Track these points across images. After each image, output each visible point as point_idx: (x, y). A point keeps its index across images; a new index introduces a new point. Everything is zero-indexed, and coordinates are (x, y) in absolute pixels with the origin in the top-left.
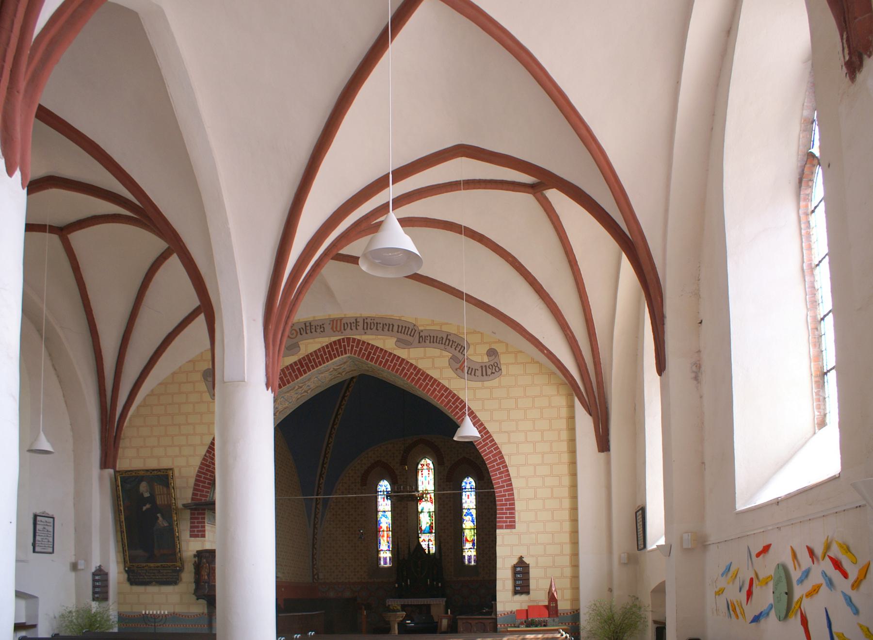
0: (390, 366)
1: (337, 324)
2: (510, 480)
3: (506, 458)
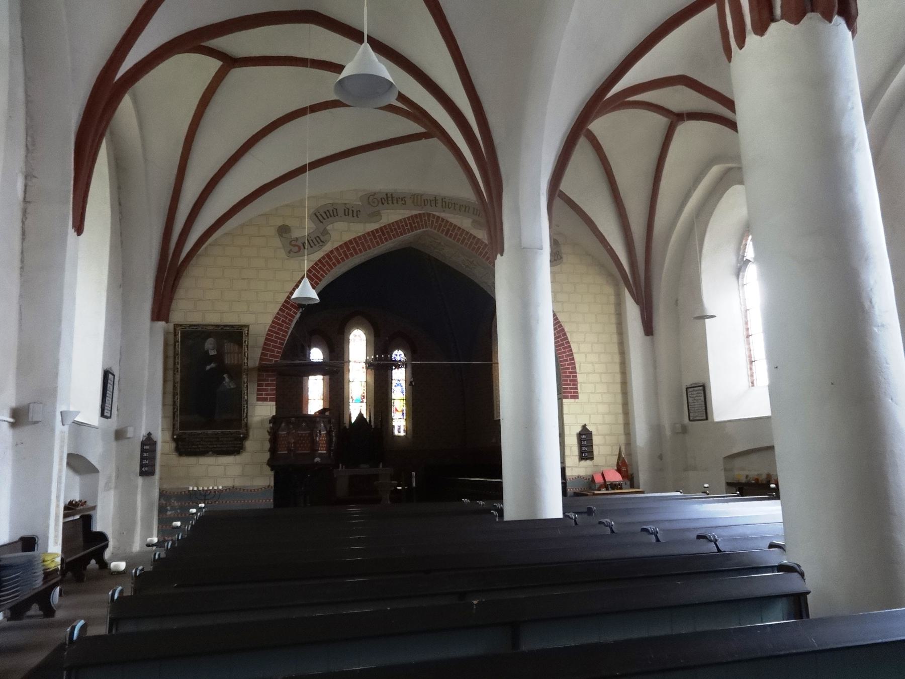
1: (418, 199)
2: (572, 355)
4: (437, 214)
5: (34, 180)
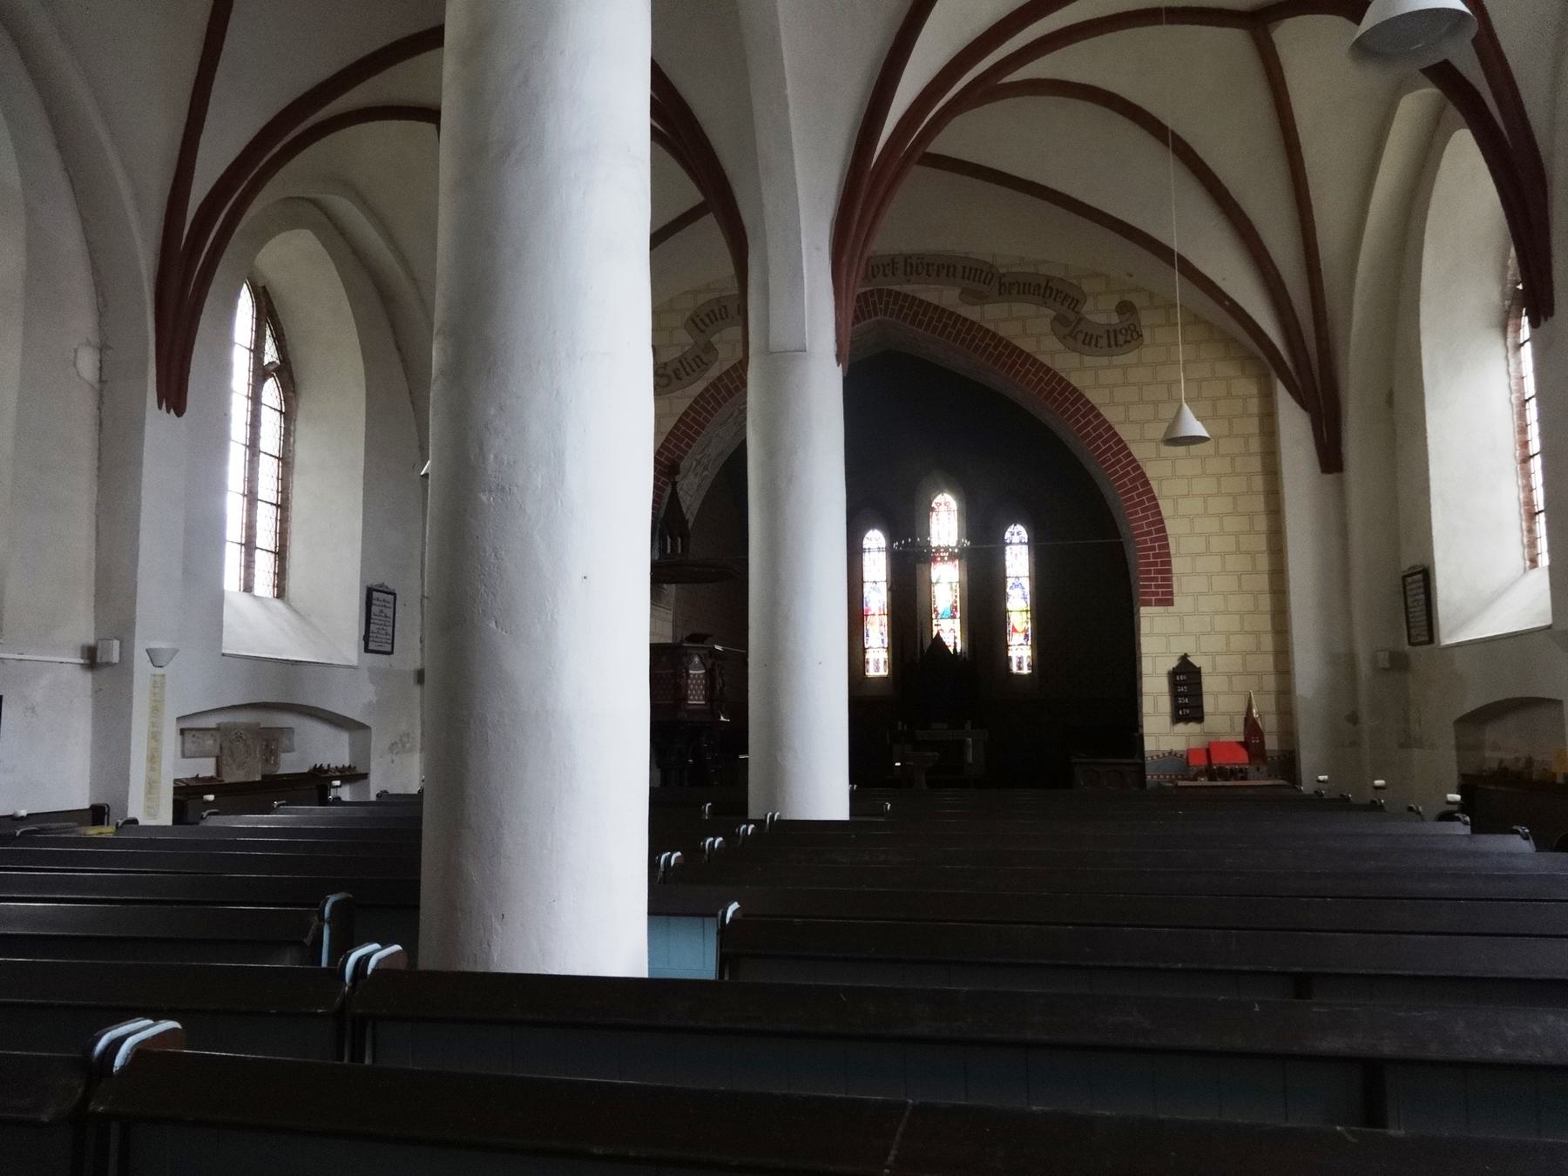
0: (964, 339)
2: (1161, 521)
3: (1153, 484)
4: (897, 288)
5: (109, 352)
